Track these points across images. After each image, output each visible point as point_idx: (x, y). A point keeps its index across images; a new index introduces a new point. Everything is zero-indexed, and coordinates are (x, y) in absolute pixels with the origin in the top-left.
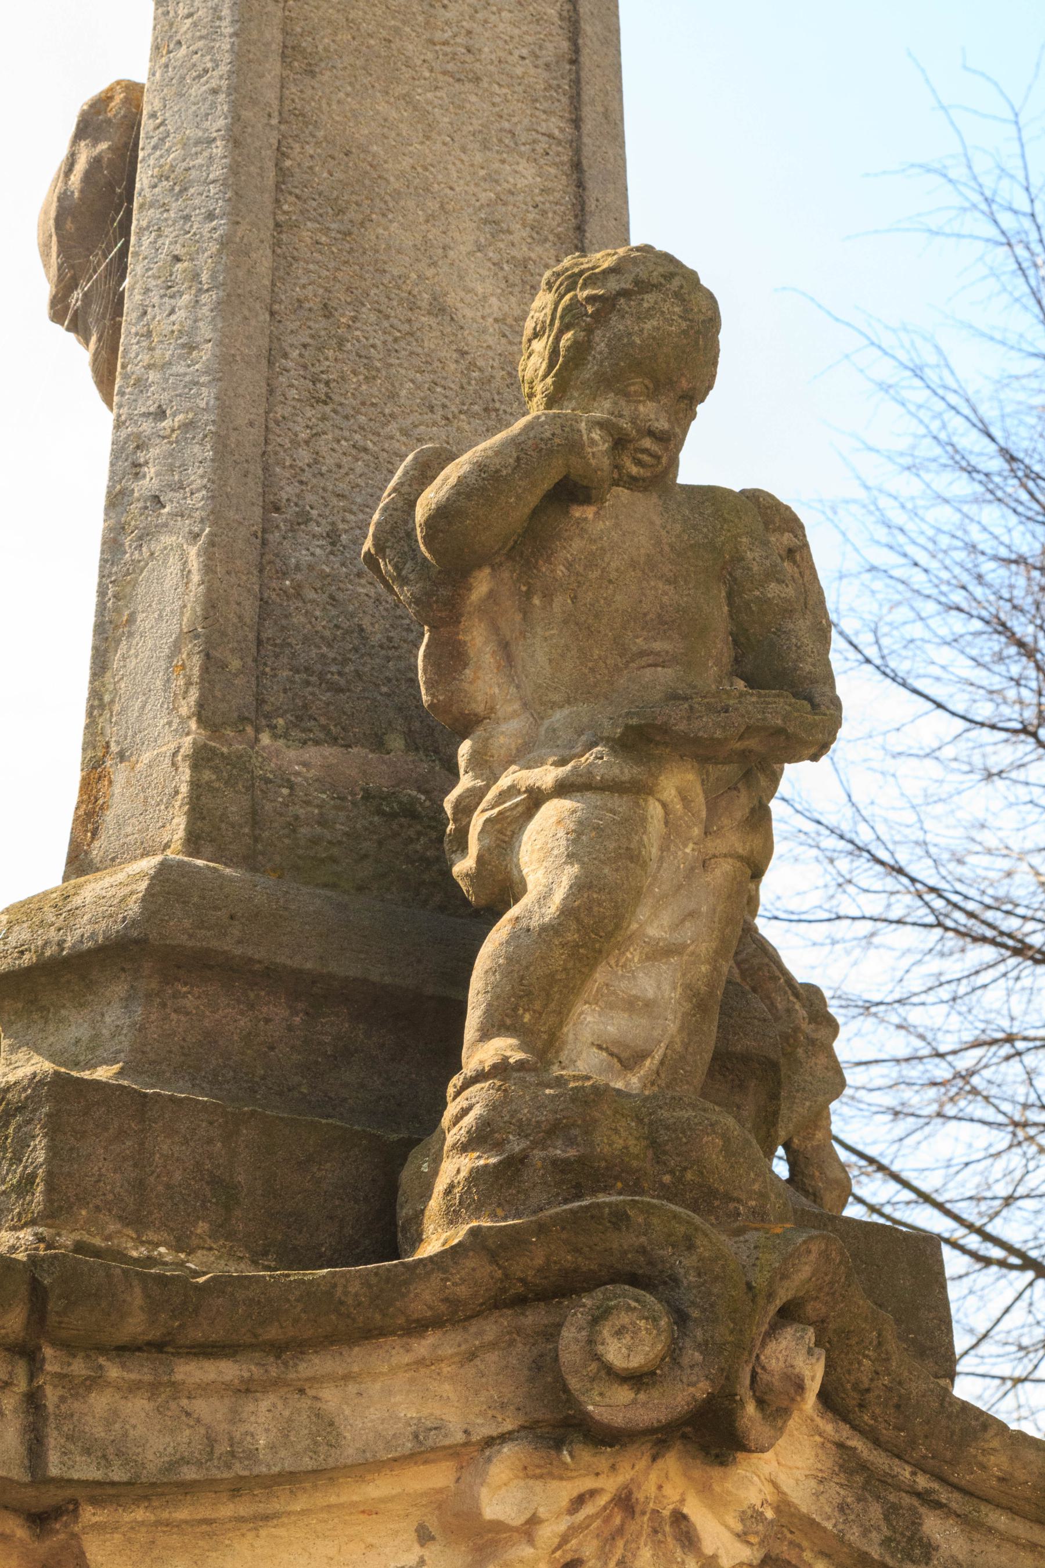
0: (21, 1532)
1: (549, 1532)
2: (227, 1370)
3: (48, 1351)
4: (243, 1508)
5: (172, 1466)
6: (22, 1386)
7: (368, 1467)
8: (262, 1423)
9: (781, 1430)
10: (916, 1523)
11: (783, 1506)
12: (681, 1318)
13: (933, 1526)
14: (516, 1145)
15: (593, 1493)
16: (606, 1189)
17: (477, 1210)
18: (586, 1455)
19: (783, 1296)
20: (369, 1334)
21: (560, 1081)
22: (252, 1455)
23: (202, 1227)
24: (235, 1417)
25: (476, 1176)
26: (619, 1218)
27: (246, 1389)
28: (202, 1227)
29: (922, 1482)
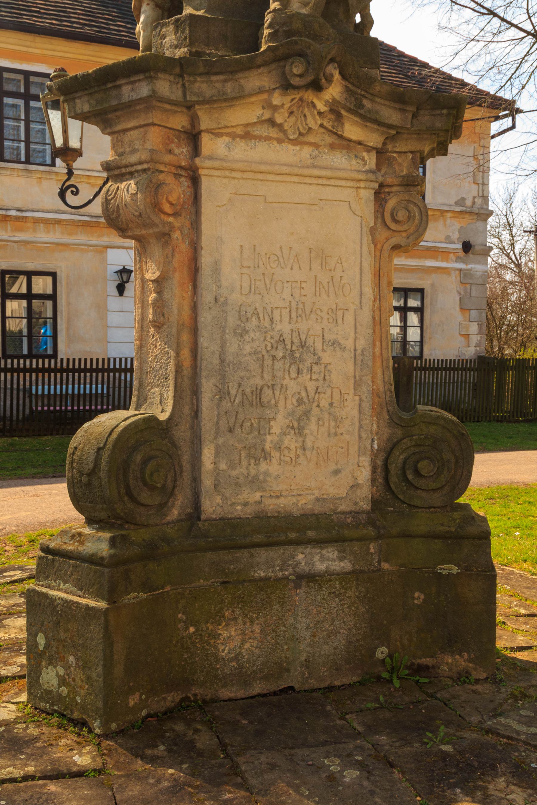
0: (185, 110)
1: (287, 106)
2: (221, 77)
3: (185, 76)
4: (227, 104)
5: (212, 97)
6: (181, 83)
7: (250, 95)
8: (229, 88)
9: (331, 84)
10: (361, 101)
11: (334, 99)
12: (309, 63)
13: (365, 102)
14: (277, 27)
15: (295, 98)
16: (294, 36)
17: (270, 42)
18: (292, 91)
19: (329, 57)
20: (249, 68)
21: (286, 13)
22: (227, 94)
23: (221, 45)
24: (223, 87)
25: (270, 34)
26: (296, 42)
27: (225, 81)
28: (221, 45)
29: (363, 93)
